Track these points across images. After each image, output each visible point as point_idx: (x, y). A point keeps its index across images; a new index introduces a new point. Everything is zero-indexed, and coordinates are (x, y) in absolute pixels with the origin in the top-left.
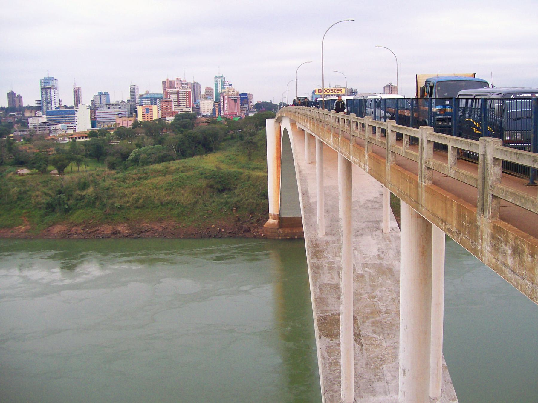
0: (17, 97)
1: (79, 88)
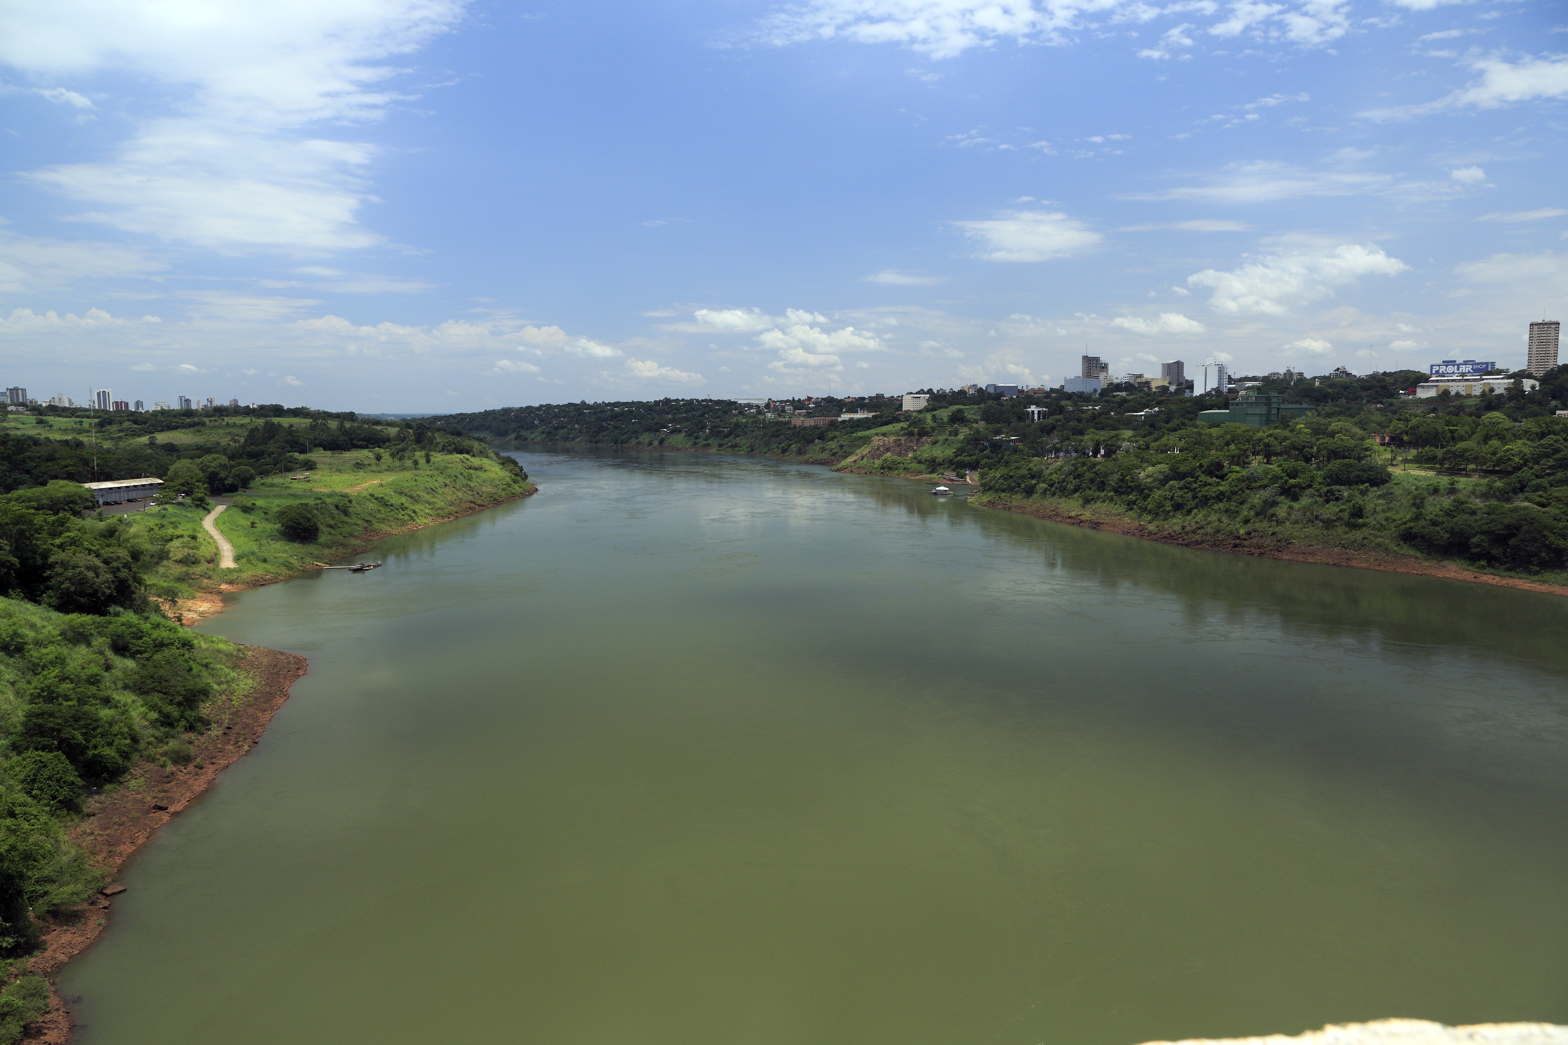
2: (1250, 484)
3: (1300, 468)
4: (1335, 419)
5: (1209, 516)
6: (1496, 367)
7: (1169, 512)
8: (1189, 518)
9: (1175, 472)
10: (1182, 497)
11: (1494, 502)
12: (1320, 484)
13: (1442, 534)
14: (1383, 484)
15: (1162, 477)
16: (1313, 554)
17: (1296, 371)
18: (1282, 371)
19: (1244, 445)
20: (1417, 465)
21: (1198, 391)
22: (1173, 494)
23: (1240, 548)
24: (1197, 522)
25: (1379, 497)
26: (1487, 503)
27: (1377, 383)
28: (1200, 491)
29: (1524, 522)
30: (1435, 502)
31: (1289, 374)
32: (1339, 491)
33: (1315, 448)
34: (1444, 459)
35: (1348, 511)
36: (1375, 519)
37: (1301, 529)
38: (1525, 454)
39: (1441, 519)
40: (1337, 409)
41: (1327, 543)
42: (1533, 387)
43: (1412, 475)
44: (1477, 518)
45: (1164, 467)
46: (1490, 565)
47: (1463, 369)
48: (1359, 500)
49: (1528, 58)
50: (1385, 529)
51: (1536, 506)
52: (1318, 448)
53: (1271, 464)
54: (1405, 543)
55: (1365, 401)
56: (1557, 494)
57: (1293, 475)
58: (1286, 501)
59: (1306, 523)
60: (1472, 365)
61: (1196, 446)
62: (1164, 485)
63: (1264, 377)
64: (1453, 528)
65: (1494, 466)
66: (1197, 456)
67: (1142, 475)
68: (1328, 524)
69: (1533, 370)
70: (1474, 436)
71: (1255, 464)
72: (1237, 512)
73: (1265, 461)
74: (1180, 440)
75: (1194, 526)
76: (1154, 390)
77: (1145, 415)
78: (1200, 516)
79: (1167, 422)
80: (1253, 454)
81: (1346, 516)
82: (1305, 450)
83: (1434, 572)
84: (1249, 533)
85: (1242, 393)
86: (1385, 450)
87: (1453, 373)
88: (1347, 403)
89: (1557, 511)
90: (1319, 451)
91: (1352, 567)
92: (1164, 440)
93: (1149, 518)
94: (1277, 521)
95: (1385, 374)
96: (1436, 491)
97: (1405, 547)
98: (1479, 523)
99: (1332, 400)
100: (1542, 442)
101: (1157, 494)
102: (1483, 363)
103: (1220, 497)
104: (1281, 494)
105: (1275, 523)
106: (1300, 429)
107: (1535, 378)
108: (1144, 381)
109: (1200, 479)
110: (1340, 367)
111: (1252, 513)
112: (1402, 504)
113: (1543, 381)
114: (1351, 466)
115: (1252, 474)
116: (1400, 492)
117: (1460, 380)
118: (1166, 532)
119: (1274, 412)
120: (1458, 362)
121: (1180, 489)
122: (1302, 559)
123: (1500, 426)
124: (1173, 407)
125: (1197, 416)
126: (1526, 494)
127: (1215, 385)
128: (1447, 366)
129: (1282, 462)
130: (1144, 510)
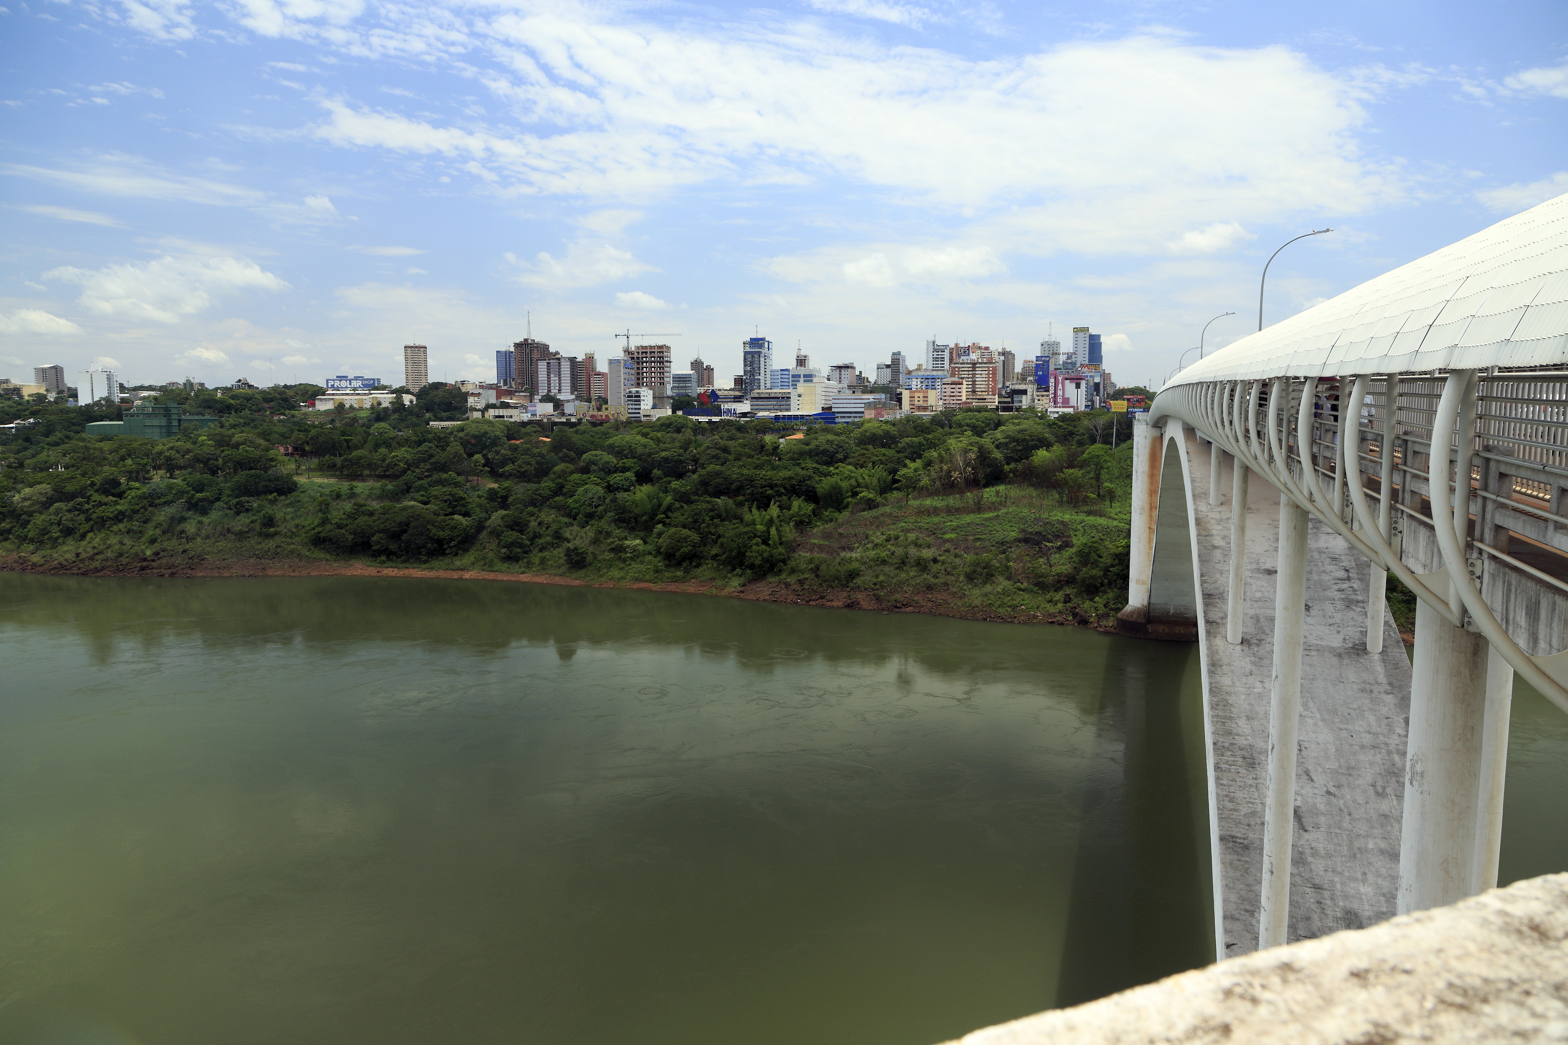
0: (705, 369)
1: (805, 357)
2: (153, 500)
3: (206, 481)
4: (238, 430)
5: (108, 539)
6: (382, 383)
7: (57, 538)
8: (83, 543)
9: (61, 492)
10: (72, 520)
11: (388, 503)
12: (229, 496)
13: (347, 536)
14: (290, 493)
15: (44, 499)
16: (228, 567)
17: (196, 381)
18: (181, 381)
19: (143, 459)
20: (320, 473)
21: (84, 399)
22: (61, 518)
23: (148, 571)
24: (94, 548)
25: (287, 506)
26: (382, 505)
27: (278, 396)
28: (94, 512)
29: (411, 519)
30: (339, 507)
31: (189, 384)
32: (248, 502)
33: (221, 460)
34: (343, 467)
35: (258, 521)
36: (286, 527)
37: (213, 544)
38: (408, 460)
39: (344, 522)
40: (242, 421)
41: (241, 555)
42: (411, 402)
43: (316, 483)
44: (375, 518)
45: (45, 488)
46: (389, 559)
47: (355, 384)
48: (269, 510)
49: (366, 109)
50: (296, 536)
51: (420, 505)
52: (223, 460)
53: (174, 478)
54: (316, 547)
55: (268, 413)
56: (435, 493)
57: (200, 488)
58: (195, 516)
59: (218, 537)
60: (362, 380)
61: (85, 462)
62: (48, 508)
63: (161, 387)
64: (355, 529)
65: (385, 471)
66: (87, 473)
67: (17, 498)
68: (241, 535)
69: (410, 387)
70: (366, 445)
71: (156, 479)
72: (141, 532)
73: (168, 475)
74: (64, 455)
75: (91, 552)
76: (26, 398)
77: (16, 427)
78: (98, 539)
79: (47, 434)
80: (154, 468)
81: (257, 526)
82: (210, 462)
83: (343, 572)
84: (156, 554)
85: (138, 403)
86: (289, 460)
87: (346, 387)
88: (251, 414)
89: (436, 508)
90: (225, 463)
91: (268, 576)
92: (42, 456)
93: (32, 547)
94: (187, 538)
95: (285, 386)
96: (338, 496)
97: (316, 551)
98: (377, 523)
99: (236, 412)
100: (420, 449)
101: (39, 519)
102: (370, 380)
103: (119, 517)
104: (189, 509)
105: (185, 539)
106: (203, 441)
107: (412, 394)
108: (11, 387)
109: (93, 498)
110: (241, 378)
111: (158, 531)
112: (309, 510)
113: (419, 396)
114: (258, 476)
115: (154, 490)
116: (307, 499)
117: (352, 394)
118: (56, 562)
119: (175, 423)
120: (350, 377)
121: (69, 511)
122: (217, 575)
123: (386, 435)
124: (53, 418)
125: (84, 428)
126: (412, 494)
127: (105, 394)
128: (340, 381)
129: (187, 476)
130: (24, 539)
